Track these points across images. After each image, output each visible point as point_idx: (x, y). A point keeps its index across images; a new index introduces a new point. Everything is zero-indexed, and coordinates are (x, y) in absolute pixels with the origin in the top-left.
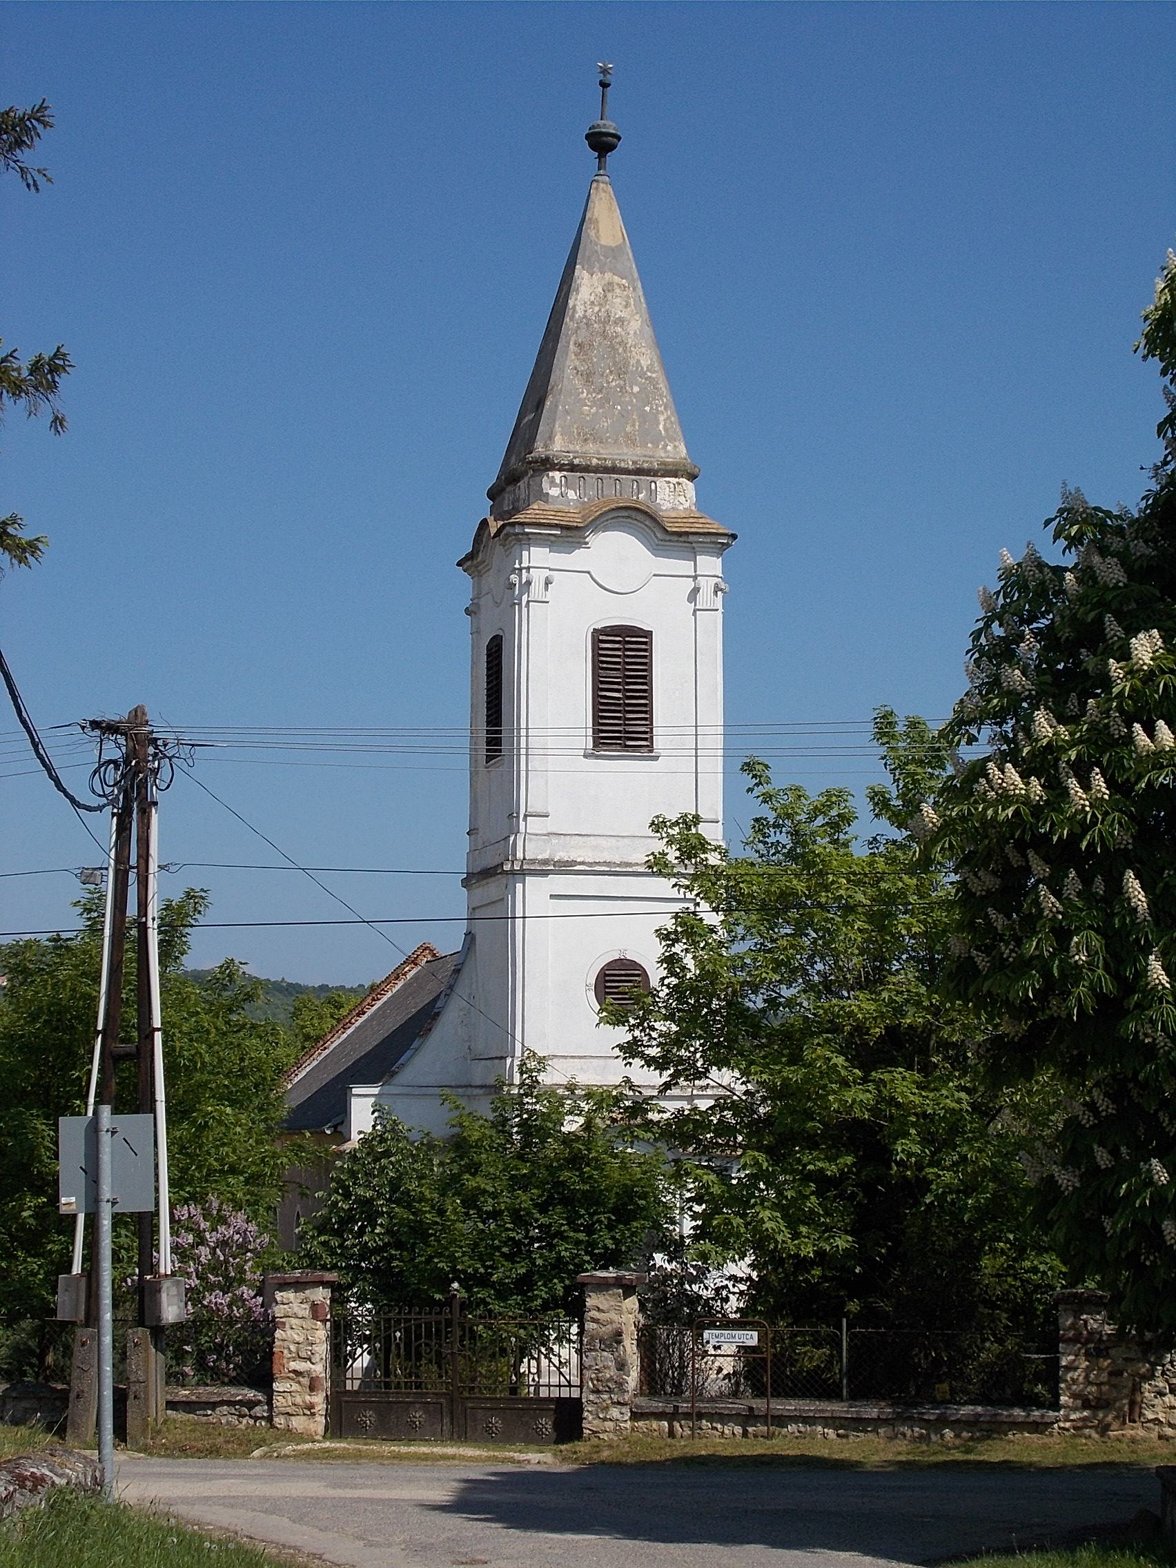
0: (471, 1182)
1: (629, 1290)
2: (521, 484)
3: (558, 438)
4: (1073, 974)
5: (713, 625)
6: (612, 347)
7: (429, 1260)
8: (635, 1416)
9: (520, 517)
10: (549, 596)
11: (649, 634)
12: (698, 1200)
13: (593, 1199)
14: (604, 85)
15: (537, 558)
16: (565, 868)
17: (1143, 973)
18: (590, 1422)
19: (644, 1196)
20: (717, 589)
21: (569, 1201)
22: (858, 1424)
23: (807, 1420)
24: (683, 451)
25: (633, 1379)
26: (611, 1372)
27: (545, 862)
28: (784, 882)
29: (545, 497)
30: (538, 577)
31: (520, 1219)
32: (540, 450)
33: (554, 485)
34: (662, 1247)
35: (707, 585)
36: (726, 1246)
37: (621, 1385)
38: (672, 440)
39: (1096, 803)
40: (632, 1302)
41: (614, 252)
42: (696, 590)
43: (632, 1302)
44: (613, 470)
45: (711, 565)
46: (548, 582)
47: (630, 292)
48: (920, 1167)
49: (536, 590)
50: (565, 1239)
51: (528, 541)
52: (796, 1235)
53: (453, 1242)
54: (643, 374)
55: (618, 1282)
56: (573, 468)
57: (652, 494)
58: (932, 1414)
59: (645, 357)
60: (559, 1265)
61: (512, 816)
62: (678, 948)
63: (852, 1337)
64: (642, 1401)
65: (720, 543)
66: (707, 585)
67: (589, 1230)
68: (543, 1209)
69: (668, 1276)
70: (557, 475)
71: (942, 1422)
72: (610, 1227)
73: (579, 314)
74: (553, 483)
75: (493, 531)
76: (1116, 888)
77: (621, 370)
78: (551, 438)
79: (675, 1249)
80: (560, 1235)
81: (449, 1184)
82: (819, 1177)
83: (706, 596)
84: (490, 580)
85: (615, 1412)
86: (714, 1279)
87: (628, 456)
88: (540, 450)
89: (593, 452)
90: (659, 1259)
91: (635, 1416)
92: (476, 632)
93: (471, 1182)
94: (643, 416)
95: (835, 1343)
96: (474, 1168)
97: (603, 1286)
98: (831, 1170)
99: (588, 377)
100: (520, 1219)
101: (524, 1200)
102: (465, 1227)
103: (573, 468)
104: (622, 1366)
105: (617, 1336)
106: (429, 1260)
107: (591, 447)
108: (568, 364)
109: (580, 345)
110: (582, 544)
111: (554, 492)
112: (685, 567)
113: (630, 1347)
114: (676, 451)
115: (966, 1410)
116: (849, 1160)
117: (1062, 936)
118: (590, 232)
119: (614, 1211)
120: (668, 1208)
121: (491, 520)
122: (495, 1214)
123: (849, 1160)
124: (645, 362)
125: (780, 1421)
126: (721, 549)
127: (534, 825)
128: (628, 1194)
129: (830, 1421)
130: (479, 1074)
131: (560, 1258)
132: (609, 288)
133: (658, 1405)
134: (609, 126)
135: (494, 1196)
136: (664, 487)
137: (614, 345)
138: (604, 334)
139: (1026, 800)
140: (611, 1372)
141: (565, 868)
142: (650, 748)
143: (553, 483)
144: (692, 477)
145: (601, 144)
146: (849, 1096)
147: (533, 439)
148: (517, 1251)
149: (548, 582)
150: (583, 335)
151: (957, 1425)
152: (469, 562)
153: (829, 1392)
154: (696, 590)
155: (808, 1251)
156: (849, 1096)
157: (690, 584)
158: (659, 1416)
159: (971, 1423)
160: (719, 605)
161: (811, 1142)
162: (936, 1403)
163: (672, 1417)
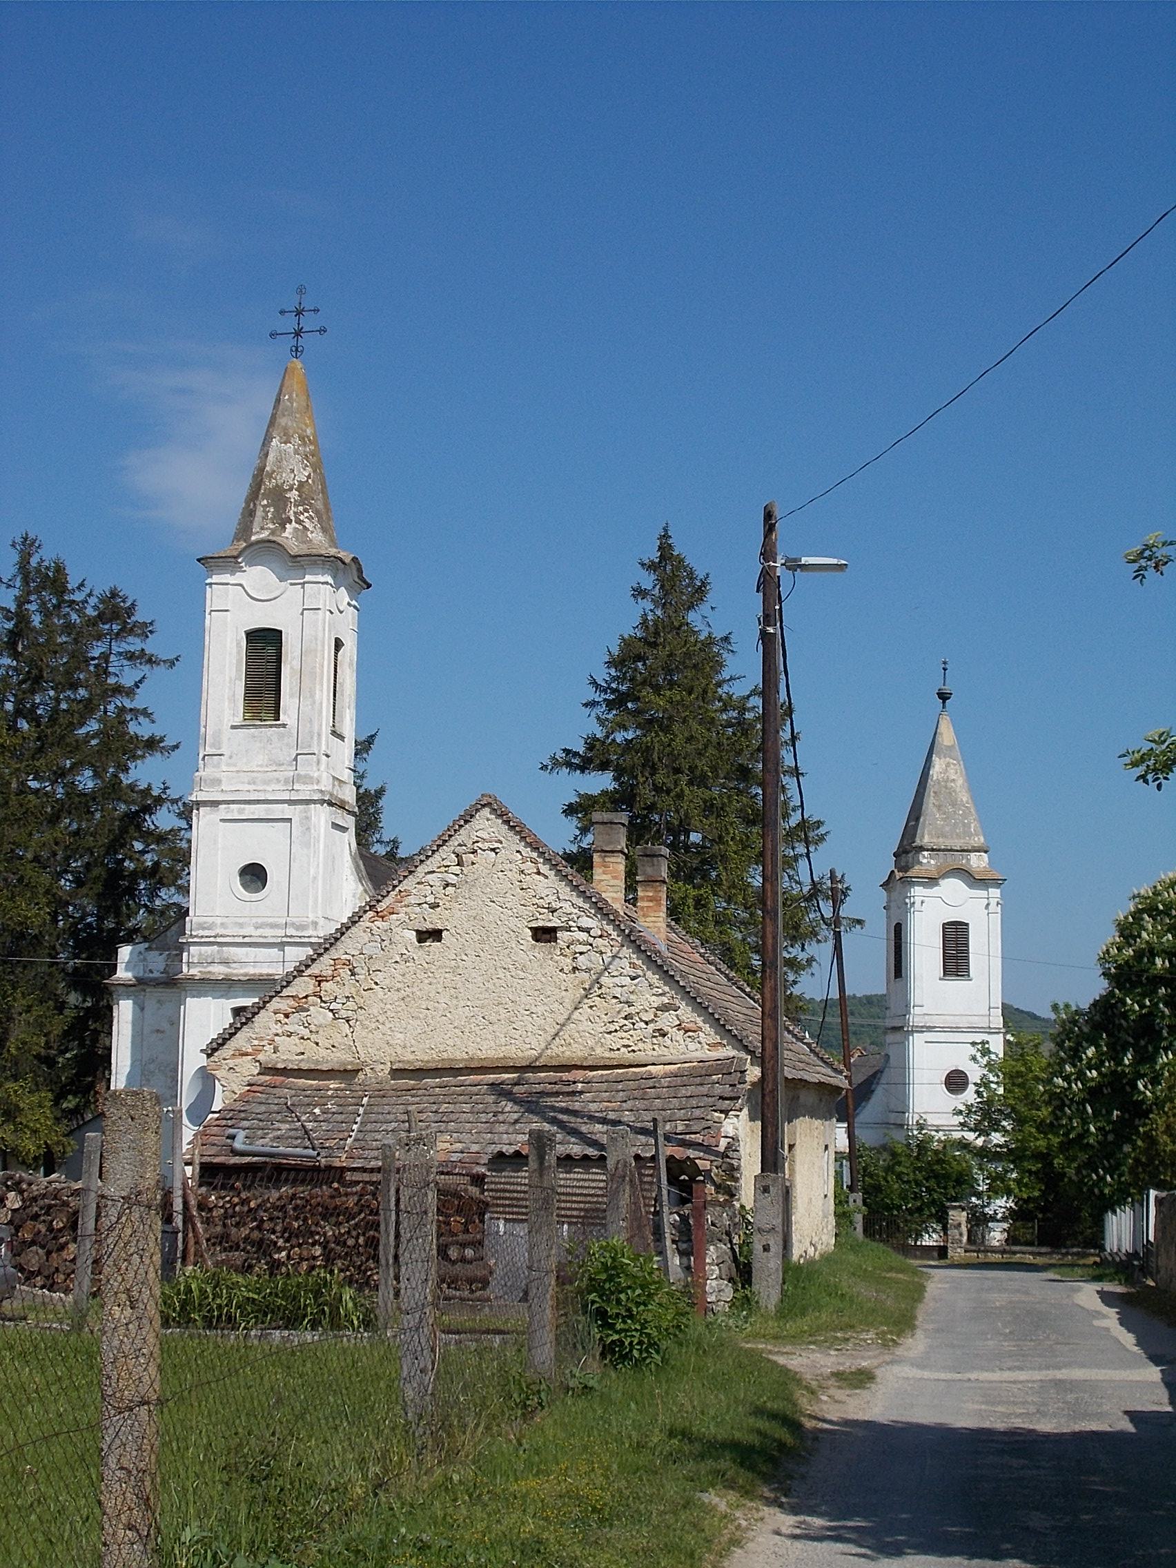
0: (898, 1169)
1: (963, 1209)
2: (910, 855)
3: (926, 837)
4: (1073, 1128)
5: (996, 919)
6: (950, 793)
7: (882, 1200)
8: (966, 1251)
9: (909, 874)
10: (923, 908)
11: (967, 925)
12: (988, 1178)
13: (947, 1177)
14: (945, 669)
15: (918, 892)
16: (930, 1029)
17: (1088, 1129)
18: (950, 1253)
19: (967, 1175)
20: (998, 903)
21: (937, 1176)
22: (1040, 1254)
23: (1023, 1253)
24: (982, 839)
25: (965, 1239)
26: (957, 1237)
27: (922, 1027)
28: (1017, 1069)
29: (921, 863)
30: (918, 900)
31: (918, 1184)
32: (918, 842)
33: (925, 857)
34: (974, 1195)
35: (993, 902)
36: (997, 1193)
37: (961, 1241)
38: (977, 835)
39: (1079, 1089)
40: (964, 1214)
41: (950, 748)
42: (988, 904)
43: (964, 1214)
44: (951, 850)
45: (995, 893)
46: (922, 902)
47: (957, 767)
48: (1063, 1168)
49: (917, 905)
50: (936, 1192)
51: (913, 884)
52: (1021, 1191)
53: (892, 1192)
54: (964, 806)
55: (960, 1206)
56: (933, 850)
57: (968, 860)
58: (1064, 1251)
59: (964, 797)
60: (933, 1202)
61: (907, 1006)
62: (981, 1089)
63: (1039, 1226)
64: (968, 1247)
65: (996, 883)
66: (993, 902)
67: (945, 1188)
68: (927, 1180)
69: (977, 1206)
70: (926, 853)
71: (1067, 1254)
72: (954, 1187)
73: (935, 778)
74: (924, 857)
75: (898, 878)
76: (1085, 1108)
77: (954, 804)
78: (923, 836)
79: (979, 1195)
80: (934, 1190)
81: (889, 1169)
82: (1030, 1172)
83: (993, 907)
84: (895, 895)
85: (959, 1250)
86: (993, 1207)
87: (957, 844)
88: (918, 842)
89: (942, 843)
90: (974, 1199)
91: (966, 1251)
92: (888, 917)
93: (898, 1169)
94: (964, 825)
95: (1033, 1227)
96: (899, 1163)
97: (955, 1208)
98: (1034, 1169)
99: (939, 807)
100: (918, 1184)
101: (919, 1176)
102: (896, 1186)
103: (933, 850)
104: (961, 1235)
105: (959, 1225)
106: (882, 1200)
107: (941, 840)
108: (930, 801)
109: (935, 793)
110: (937, 884)
111: (925, 861)
112: (983, 893)
113: (964, 1229)
114: (979, 840)
115: (1075, 1250)
116: (1040, 1165)
117: (1070, 1119)
118: (939, 739)
119: (955, 1181)
120: (976, 1180)
121: (896, 871)
122: (908, 1182)
123: (1040, 1165)
124: (965, 799)
125: (1015, 1253)
126: (998, 886)
127: (917, 1010)
128: (960, 1174)
129: (1030, 1253)
130: (893, 1118)
131: (934, 1199)
132: (948, 765)
133: (973, 1248)
134: (947, 689)
135: (908, 1174)
136: (973, 856)
137: (951, 792)
138: (946, 787)
139: (1063, 1087)
140: (957, 1237)
141: (930, 1029)
142: (969, 976)
143: (924, 857)
144: (986, 852)
145: (944, 697)
146: (1038, 1143)
147: (915, 835)
148: (917, 1197)
149: (922, 902)
150: (936, 788)
151: (1073, 1254)
152: (885, 885)
153: (1030, 1244)
154: (988, 904)
155: (1025, 1196)
156: (1038, 1143)
157: (986, 901)
158: (974, 1251)
159: (1077, 1254)
160: (999, 911)
161: (1029, 1158)
162: (1065, 1248)
163: (978, 1252)
